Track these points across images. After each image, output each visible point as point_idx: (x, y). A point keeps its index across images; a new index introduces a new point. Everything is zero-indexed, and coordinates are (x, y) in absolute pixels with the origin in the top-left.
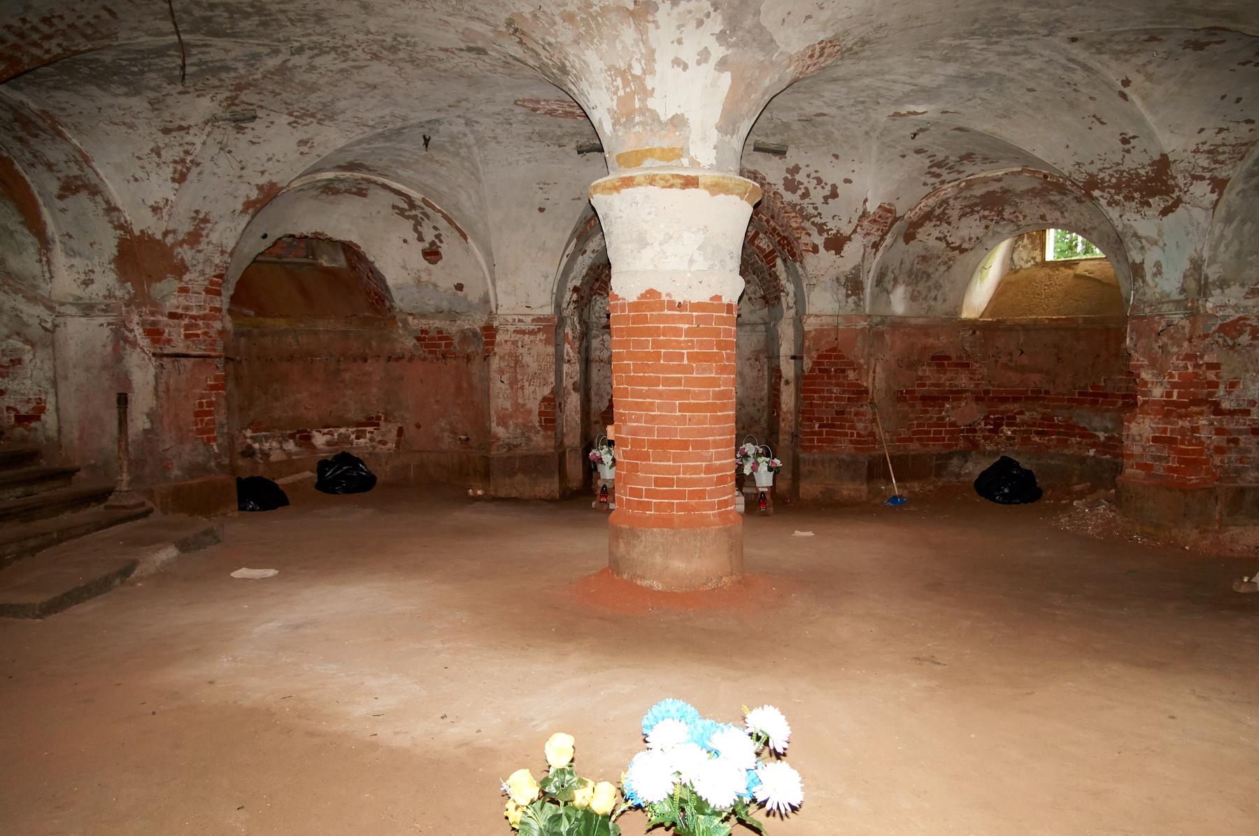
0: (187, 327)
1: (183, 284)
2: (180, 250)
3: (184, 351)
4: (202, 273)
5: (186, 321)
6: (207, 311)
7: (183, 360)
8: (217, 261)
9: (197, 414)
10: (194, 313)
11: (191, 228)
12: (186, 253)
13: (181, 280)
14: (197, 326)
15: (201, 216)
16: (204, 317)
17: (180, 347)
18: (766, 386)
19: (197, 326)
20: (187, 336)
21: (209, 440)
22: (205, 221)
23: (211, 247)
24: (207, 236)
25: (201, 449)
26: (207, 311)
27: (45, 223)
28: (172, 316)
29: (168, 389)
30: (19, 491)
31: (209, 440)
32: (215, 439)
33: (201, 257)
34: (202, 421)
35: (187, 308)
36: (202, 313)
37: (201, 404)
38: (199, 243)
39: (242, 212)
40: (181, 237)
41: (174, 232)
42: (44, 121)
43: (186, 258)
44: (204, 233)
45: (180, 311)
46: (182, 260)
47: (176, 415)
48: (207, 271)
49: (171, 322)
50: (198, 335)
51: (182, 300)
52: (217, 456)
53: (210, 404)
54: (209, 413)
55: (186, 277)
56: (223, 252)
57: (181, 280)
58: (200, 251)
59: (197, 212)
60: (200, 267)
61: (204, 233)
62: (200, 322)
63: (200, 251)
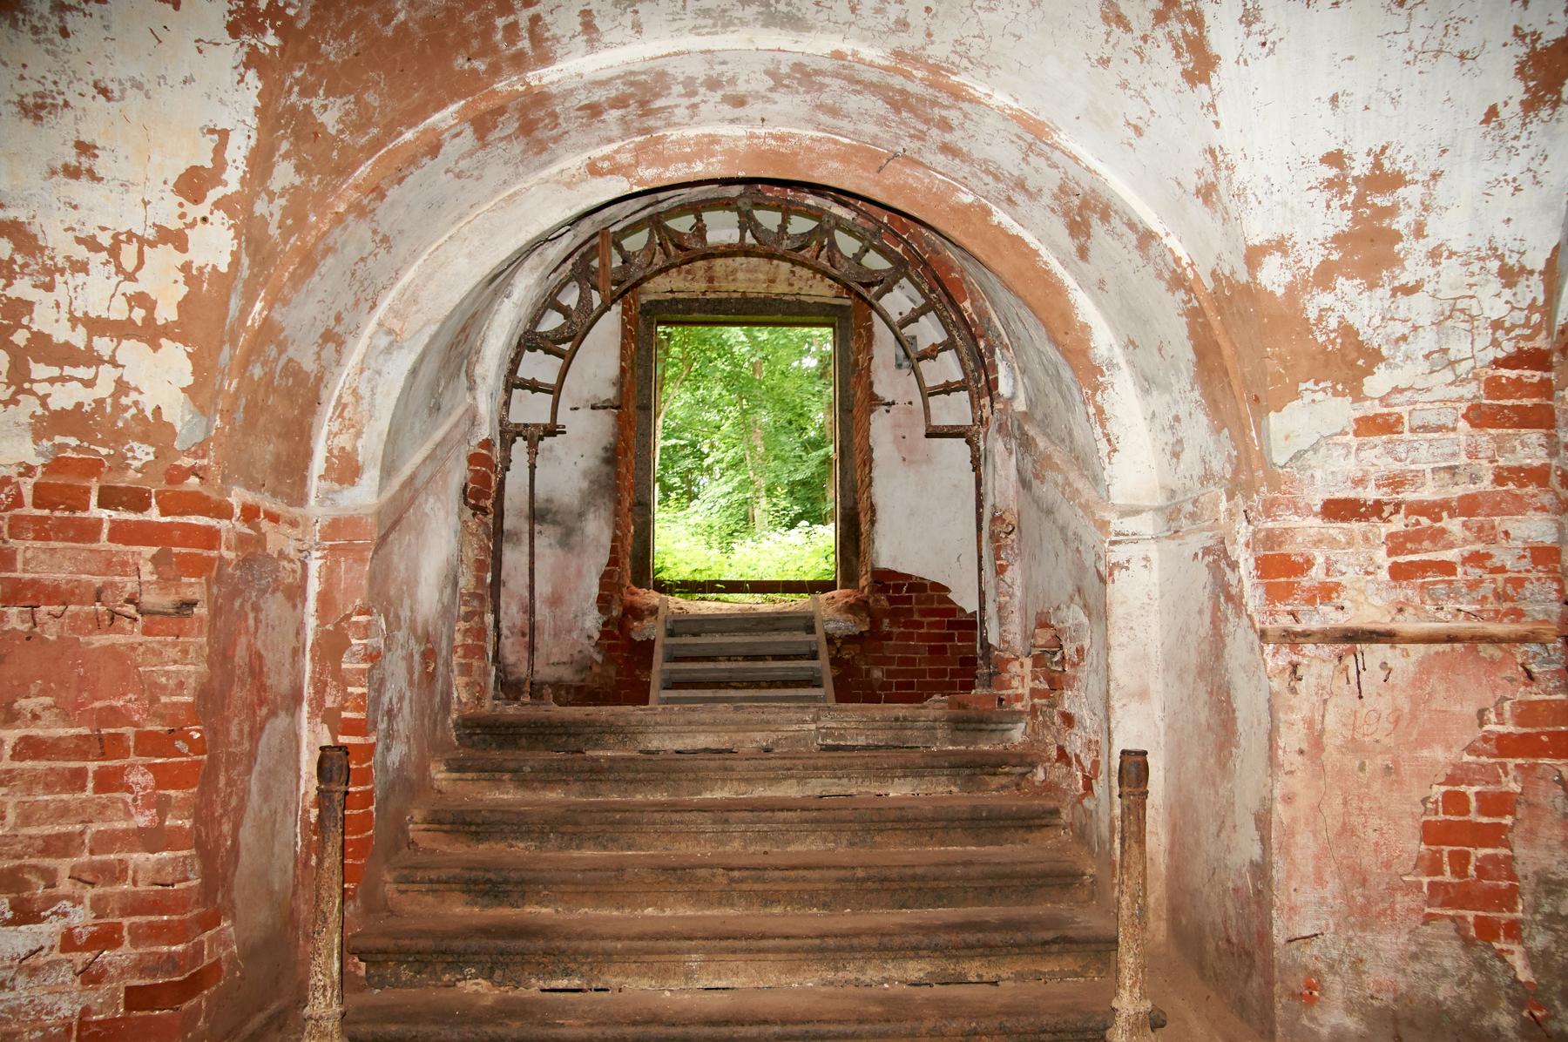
0: (1396, 544)
1: (1372, 408)
2: (1325, 299)
3: (1384, 622)
4: (1441, 358)
5: (1398, 524)
6: (1486, 484)
7: (1376, 653)
8: (1498, 310)
9: (1431, 833)
10: (1428, 493)
11: (1342, 221)
12: (1354, 305)
13: (1358, 396)
14: (1438, 536)
15: (1360, 167)
16: (1468, 506)
17: (1368, 605)
18: (61, 576)
19: (1438, 537)
20: (1398, 572)
21: (1487, 930)
22: (1384, 180)
23: (1451, 270)
24: (1419, 231)
25: (1450, 955)
26: (1486, 484)
27: (1086, 328)
28: (1337, 510)
29: (1317, 742)
30: (916, 969)
31: (1487, 930)
32: (1514, 931)
33: (1421, 308)
34: (1459, 862)
35: (1396, 482)
36: (1457, 491)
37: (1455, 801)
38: (1394, 261)
39: (1530, 106)
40: (1313, 259)
41: (1280, 245)
42: (908, 76)
43: (1355, 320)
44: (1401, 223)
45: (1370, 494)
46: (1347, 331)
47: (1347, 830)
48: (1460, 347)
49: (1336, 529)
50: (1447, 568)
51: (1377, 458)
52: (1523, 996)
53: (1497, 803)
54: (1494, 835)
55: (1377, 383)
56: (1510, 276)
57: (1358, 396)
58: (1408, 290)
59: (1335, 159)
60: (1427, 341)
61: (1401, 223)
62: (1454, 525)
63: (1408, 290)
